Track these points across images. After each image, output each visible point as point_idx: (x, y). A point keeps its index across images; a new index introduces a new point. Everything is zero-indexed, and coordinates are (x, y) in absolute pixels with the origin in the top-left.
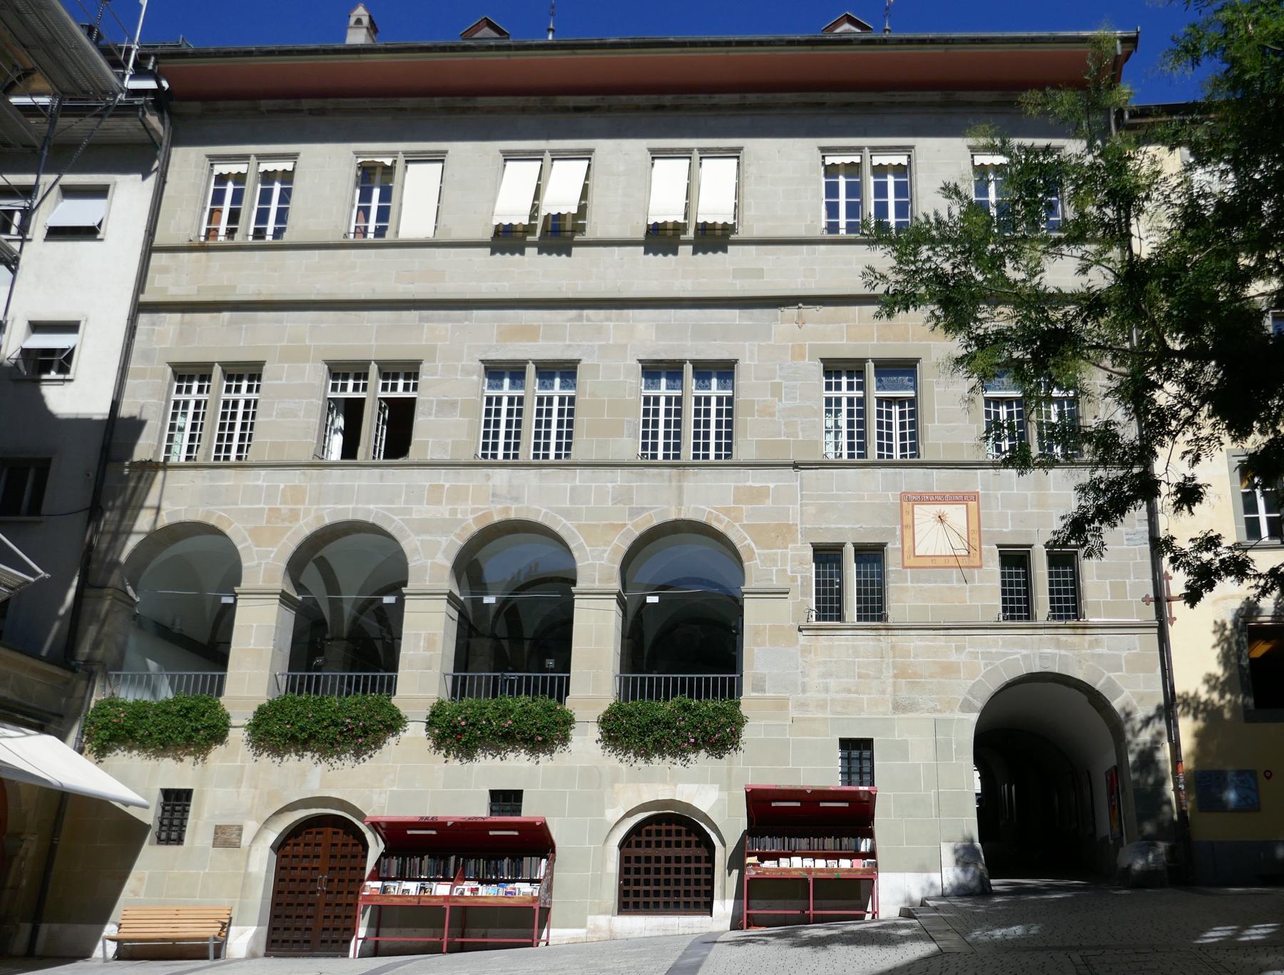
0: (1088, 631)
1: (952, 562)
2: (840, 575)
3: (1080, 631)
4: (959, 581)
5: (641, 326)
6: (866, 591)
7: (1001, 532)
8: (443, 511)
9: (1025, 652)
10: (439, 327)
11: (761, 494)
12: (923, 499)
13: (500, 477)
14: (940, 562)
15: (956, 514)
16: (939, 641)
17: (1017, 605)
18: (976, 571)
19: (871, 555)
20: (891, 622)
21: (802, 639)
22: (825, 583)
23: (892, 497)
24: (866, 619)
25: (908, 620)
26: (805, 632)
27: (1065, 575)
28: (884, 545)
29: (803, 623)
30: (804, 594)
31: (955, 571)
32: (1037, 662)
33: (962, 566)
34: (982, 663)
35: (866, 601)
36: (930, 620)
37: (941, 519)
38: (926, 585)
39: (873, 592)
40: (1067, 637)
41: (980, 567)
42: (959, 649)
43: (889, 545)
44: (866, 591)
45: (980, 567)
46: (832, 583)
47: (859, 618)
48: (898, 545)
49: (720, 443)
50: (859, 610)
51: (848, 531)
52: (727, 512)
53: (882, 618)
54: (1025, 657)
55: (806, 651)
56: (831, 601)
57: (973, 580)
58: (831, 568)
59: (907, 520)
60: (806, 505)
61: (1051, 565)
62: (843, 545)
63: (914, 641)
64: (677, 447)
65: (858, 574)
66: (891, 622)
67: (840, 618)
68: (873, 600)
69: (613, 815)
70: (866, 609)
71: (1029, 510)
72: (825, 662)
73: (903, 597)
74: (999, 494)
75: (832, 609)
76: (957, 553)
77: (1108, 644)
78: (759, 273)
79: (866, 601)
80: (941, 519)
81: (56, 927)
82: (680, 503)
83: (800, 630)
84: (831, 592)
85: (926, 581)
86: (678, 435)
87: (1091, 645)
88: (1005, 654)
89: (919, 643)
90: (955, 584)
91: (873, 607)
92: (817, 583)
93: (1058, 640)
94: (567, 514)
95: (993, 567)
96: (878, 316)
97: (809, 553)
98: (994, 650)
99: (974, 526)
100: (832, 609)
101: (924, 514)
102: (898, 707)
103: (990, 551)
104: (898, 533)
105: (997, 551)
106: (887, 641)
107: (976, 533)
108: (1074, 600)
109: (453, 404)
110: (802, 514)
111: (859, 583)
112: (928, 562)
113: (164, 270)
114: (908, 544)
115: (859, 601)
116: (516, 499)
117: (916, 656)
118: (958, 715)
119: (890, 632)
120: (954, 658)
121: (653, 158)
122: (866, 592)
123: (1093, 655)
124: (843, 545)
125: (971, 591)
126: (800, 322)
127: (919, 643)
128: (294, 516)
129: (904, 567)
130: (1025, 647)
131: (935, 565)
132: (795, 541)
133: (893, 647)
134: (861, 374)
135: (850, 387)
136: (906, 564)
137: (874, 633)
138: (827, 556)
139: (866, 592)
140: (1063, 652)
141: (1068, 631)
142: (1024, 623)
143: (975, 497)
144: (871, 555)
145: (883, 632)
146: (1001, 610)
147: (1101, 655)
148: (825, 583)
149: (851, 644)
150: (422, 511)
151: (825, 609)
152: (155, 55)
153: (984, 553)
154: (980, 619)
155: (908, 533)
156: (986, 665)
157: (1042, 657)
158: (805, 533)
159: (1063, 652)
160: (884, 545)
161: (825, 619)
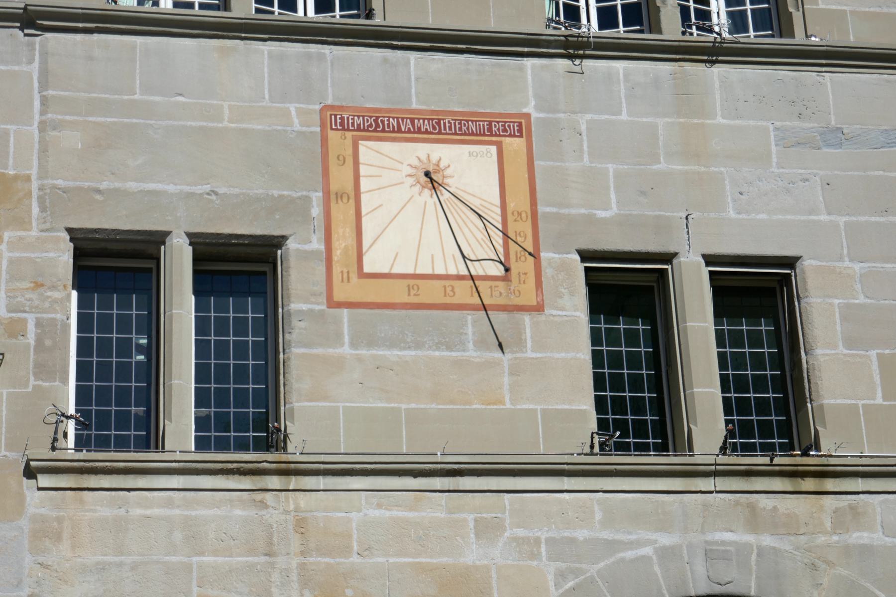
0: (830, 484)
1: (463, 293)
2: (152, 325)
3: (809, 484)
4: (480, 344)
6: (104, 368)
7: (590, 220)
9: (665, 540)
12: (382, 126)
14: (432, 293)
15: (472, 169)
16: (430, 508)
18: (527, 319)
19: (240, 270)
20: (295, 451)
21: (34, 499)
22: (105, 347)
23: (300, 118)
24: (222, 445)
25: (344, 444)
26: (44, 480)
27: (755, 340)
28: (277, 242)
29: (41, 452)
30: (44, 370)
31: (470, 317)
32: (700, 568)
33: (488, 304)
34: (550, 570)
35: (222, 398)
36: (405, 446)
37: (431, 179)
38: (394, 354)
39: (241, 374)
40: (778, 502)
41: (539, 308)
42: (487, 530)
43: (292, 244)
44: (104, 368)
45: (539, 308)
46: (125, 348)
47: (202, 444)
48: (317, 244)
50: (201, 423)
51: (179, 198)
53: (270, 438)
54: (666, 554)
55: (45, 533)
56: (123, 396)
57: (520, 343)
58: (124, 305)
59: (340, 178)
60: (56, 126)
61: (719, 313)
62: (159, 238)
63: (361, 511)
65: (201, 326)
66: (295, 451)
67: (151, 438)
68: (241, 398)
70: (223, 423)
71: (662, 166)
72: (102, 568)
74: (583, 121)
75: (123, 421)
76: (477, 269)
79: (222, 398)
80: (431, 179)
83: (30, 473)
84: (124, 371)
85: (392, 344)
87: (840, 523)
88: (612, 546)
89: (375, 513)
90: (472, 353)
91: (246, 418)
92: (83, 346)
93: (752, 507)
95: (573, 306)
96: (170, 420)
97: (63, 258)
98: (581, 534)
99: (519, 201)
100: (123, 421)
101: (386, 168)
103: (563, 267)
104: (316, 211)
105: (579, 268)
106: (283, 506)
108: (782, 406)
110: (44, 150)
111: (202, 349)
112: (398, 293)
114: (343, 241)
115: (201, 399)
117: (366, 550)
119: (294, 482)
120: (473, 554)
122: (222, 374)
123: (847, 550)
124: (159, 238)
125: (514, 372)
127: (375, 513)
129: (333, 304)
130: (664, 526)
131: (416, 301)
132: (23, 223)
133: (301, 525)
136: (339, 295)
137: (246, 482)
138: (113, 267)
139: (222, 374)
140: (767, 541)
141: (778, 484)
142: (652, 460)
143: (520, 127)
144: (240, 270)
145: (274, 482)
146: (594, 426)
147: (866, 550)
148: (105, 347)
151: (103, 421)
152: (267, 437)
153: (548, 272)
154: (542, 447)
155: (342, 212)
156: (561, 576)
157: (711, 554)
158: (52, 200)
159: (767, 541)
160: (277, 242)
161: (103, 444)
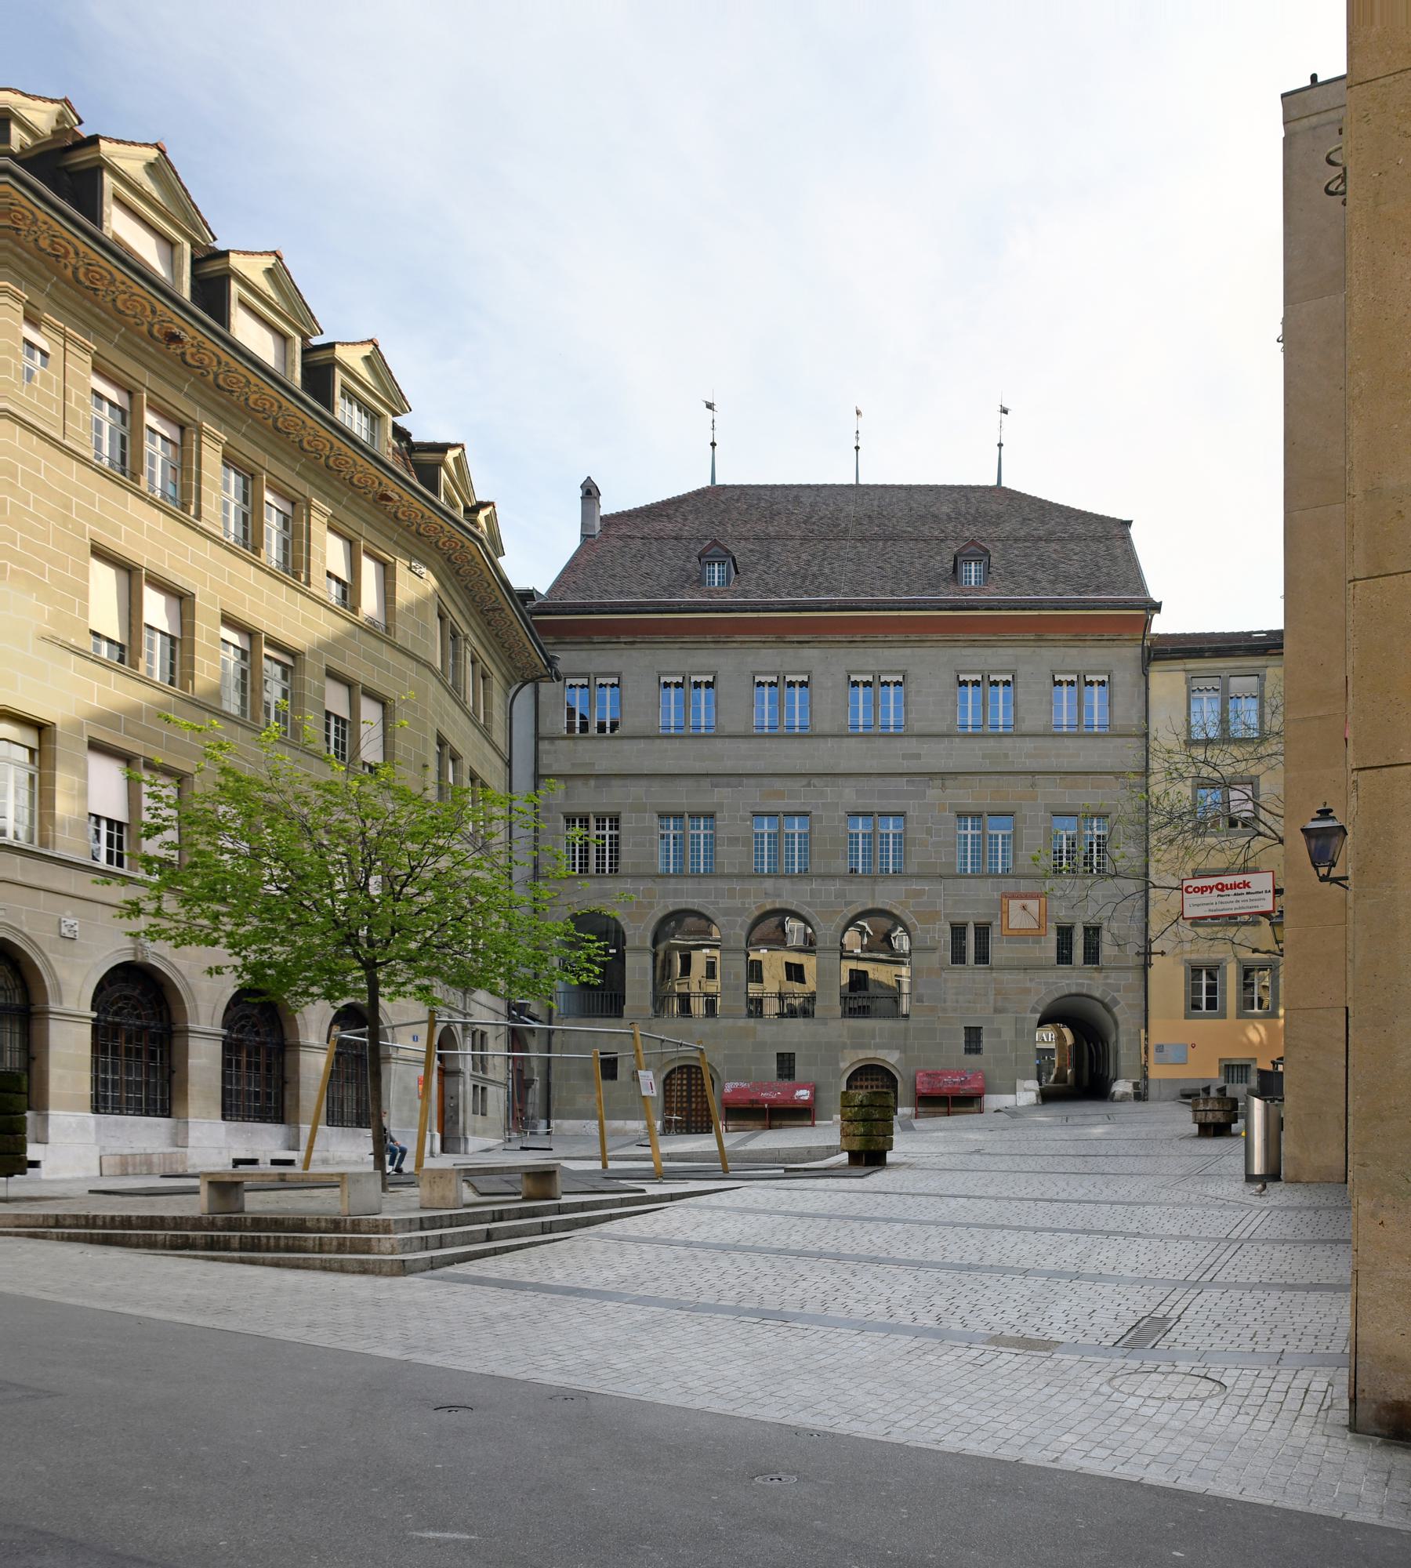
5: (847, 790)
8: (737, 903)
10: (637, 790)
11: (919, 894)
12: (1014, 897)
13: (586, 884)
15: (1033, 905)
17: (1064, 956)
19: (983, 931)
23: (996, 895)
37: (1024, 908)
49: (612, 862)
51: (971, 916)
52: (901, 903)
59: (1005, 908)
63: (1006, 977)
64: (587, 864)
69: (843, 1065)
73: (998, 951)
77: (1113, 978)
78: (918, 756)
80: (1024, 908)
81: (558, 1121)
82: (873, 897)
86: (587, 858)
94: (809, 904)
95: (1053, 936)
101: (1015, 905)
102: (997, 1011)
107: (1044, 915)
109: (737, 839)
113: (548, 752)
116: (779, 896)
118: (1029, 1015)
120: (1028, 985)
121: (1190, 691)
126: (943, 787)
128: (651, 905)
131: (1022, 936)
134: (587, 821)
135: (675, 828)
149: (970, 974)
150: (724, 903)
158: (947, 916)
